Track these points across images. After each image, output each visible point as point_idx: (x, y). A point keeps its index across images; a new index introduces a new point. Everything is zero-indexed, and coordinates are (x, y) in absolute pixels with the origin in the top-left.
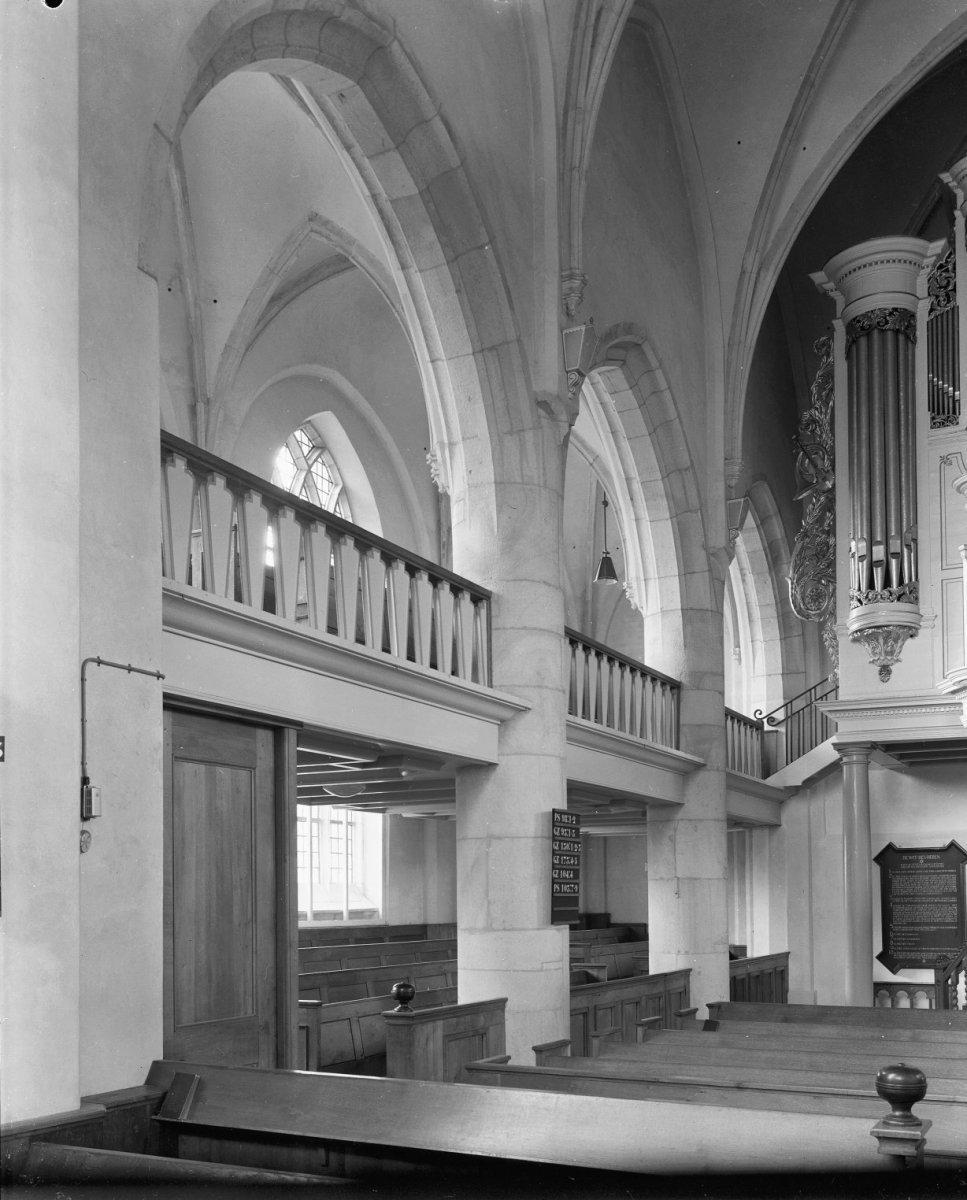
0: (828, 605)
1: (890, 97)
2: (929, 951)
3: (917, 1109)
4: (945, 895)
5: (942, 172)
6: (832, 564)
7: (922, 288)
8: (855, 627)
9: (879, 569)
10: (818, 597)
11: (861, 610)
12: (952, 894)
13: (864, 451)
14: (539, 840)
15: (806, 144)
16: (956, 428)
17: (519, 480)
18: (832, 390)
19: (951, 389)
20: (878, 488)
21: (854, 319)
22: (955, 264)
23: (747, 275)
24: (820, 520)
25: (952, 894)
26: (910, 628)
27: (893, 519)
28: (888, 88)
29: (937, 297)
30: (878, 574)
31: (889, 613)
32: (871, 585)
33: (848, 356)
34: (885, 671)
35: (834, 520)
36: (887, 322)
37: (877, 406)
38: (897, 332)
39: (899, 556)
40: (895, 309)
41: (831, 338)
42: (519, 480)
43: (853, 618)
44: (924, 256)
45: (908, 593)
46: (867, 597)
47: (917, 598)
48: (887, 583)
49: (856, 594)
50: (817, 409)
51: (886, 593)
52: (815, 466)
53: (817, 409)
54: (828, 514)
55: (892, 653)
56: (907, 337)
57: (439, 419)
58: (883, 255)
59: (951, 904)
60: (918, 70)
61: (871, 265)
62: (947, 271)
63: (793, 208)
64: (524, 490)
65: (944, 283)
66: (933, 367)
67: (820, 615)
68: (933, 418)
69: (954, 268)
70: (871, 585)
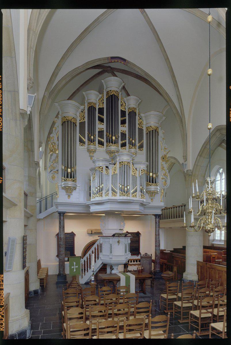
7: (78, 114)
55: (71, 193)
65: (83, 115)
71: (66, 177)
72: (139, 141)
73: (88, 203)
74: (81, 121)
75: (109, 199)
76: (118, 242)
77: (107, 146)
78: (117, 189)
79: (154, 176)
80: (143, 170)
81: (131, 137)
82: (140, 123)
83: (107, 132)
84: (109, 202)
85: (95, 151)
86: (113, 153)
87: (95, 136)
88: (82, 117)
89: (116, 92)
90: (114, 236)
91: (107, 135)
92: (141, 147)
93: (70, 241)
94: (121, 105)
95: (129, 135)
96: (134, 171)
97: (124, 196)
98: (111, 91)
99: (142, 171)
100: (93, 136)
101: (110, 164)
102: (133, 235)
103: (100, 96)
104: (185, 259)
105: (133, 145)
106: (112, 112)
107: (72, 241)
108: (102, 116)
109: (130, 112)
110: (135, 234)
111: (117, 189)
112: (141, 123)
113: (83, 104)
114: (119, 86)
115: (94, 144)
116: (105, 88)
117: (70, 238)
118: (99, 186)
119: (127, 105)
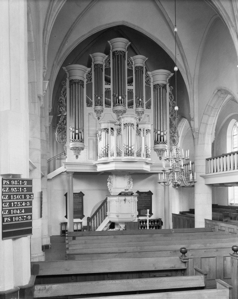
0: (64, 141)
1: (84, 37)
2: (76, 215)
3: (186, 254)
4: (79, 203)
5: (90, 54)
6: (65, 132)
7: (85, 77)
8: (71, 147)
9: (77, 135)
10: (62, 139)
11: (73, 143)
12: (81, 203)
13: (74, 109)
14: (38, 198)
15: (68, 41)
16: (91, 108)
17: (34, 114)
18: (66, 93)
19: (91, 99)
20: (77, 117)
21: (72, 80)
22: (92, 73)
23: (55, 66)
24: (63, 122)
25: (81, 203)
26: (83, 148)
27: (80, 125)
28: (85, 35)
29: (88, 79)
30: (77, 136)
31: (79, 145)
32: (75, 138)
33: (70, 87)
34: (77, 157)
35: (66, 122)
36: (79, 83)
37: (77, 100)
38: (81, 85)
39: (81, 132)
40: (81, 80)
41: (66, 82)
42: (34, 114)
43: (71, 145)
44: (86, 70)
45: (82, 141)
46: (74, 141)
47: (84, 142)
48: (79, 138)
49: (72, 139)
50: (62, 97)
51: (78, 140)
52: (62, 109)
53: (62, 97)
54: (65, 121)
55: (79, 153)
56: (83, 86)
57: (82, 117)
58: (79, 68)
59: (80, 205)
60: (90, 34)
61: (75, 69)
62: (90, 74)
63: (64, 54)
64: (35, 116)
65: (90, 77)
66: (87, 94)
67: (63, 143)
68: (87, 105)
69: (92, 74)
70: (75, 138)
71: (74, 138)
72: (147, 100)
73: (94, 163)
74: (88, 82)
75: (114, 159)
76: (125, 200)
77: (114, 106)
78: (122, 150)
79: (162, 134)
80: (147, 130)
81: (138, 96)
82: (147, 81)
83: (114, 92)
84: (114, 161)
85: (102, 111)
86: (120, 113)
87: (102, 96)
88: (89, 79)
89: (122, 52)
90: (120, 194)
91: (113, 95)
92: (148, 106)
93: (148, 200)
94: (128, 64)
95: (136, 94)
96: (138, 131)
97: (128, 156)
98: (117, 51)
99: (146, 130)
100: (100, 97)
101: (115, 125)
102: (75, 196)
103: (107, 56)
104: (194, 218)
105: (140, 104)
106: (118, 71)
107: (150, 200)
108: (109, 76)
109: (137, 71)
110: (77, 195)
111: (122, 150)
112: (148, 81)
113: (89, 66)
114: (126, 46)
115: (101, 105)
116: (111, 49)
117: (148, 197)
118: (104, 147)
119: (133, 64)
